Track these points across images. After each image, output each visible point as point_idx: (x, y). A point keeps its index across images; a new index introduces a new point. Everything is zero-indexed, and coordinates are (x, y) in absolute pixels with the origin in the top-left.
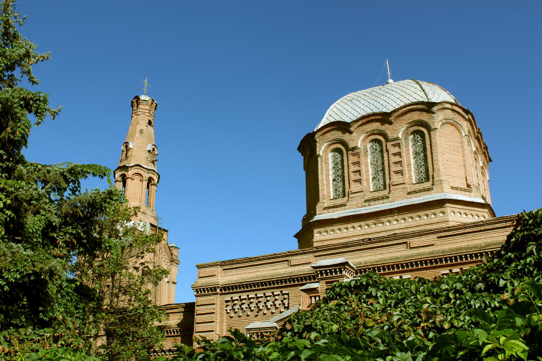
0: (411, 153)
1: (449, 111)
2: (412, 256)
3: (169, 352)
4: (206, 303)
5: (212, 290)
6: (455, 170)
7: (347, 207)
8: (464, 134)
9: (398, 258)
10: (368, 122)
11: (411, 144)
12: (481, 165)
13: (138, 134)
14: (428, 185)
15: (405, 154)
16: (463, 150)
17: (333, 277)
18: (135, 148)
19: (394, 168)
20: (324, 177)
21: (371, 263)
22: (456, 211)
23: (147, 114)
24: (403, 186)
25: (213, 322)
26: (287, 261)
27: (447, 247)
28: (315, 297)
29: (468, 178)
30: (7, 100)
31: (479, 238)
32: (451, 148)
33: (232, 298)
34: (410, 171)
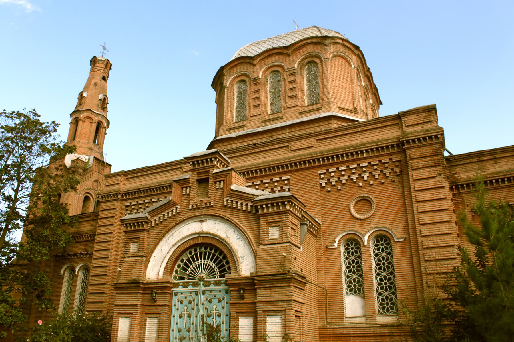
0: (305, 80)
1: (340, 46)
2: (292, 158)
3: (80, 255)
4: (108, 208)
6: (344, 96)
7: (245, 128)
8: (353, 66)
9: (278, 160)
11: (305, 73)
12: (371, 102)
15: (299, 81)
16: (352, 80)
20: (229, 104)
21: (254, 165)
23: (102, 71)
25: (112, 225)
26: (181, 168)
27: (325, 148)
28: (186, 188)
29: (355, 103)
31: (355, 138)
32: (341, 76)
33: (131, 203)
34: (303, 95)
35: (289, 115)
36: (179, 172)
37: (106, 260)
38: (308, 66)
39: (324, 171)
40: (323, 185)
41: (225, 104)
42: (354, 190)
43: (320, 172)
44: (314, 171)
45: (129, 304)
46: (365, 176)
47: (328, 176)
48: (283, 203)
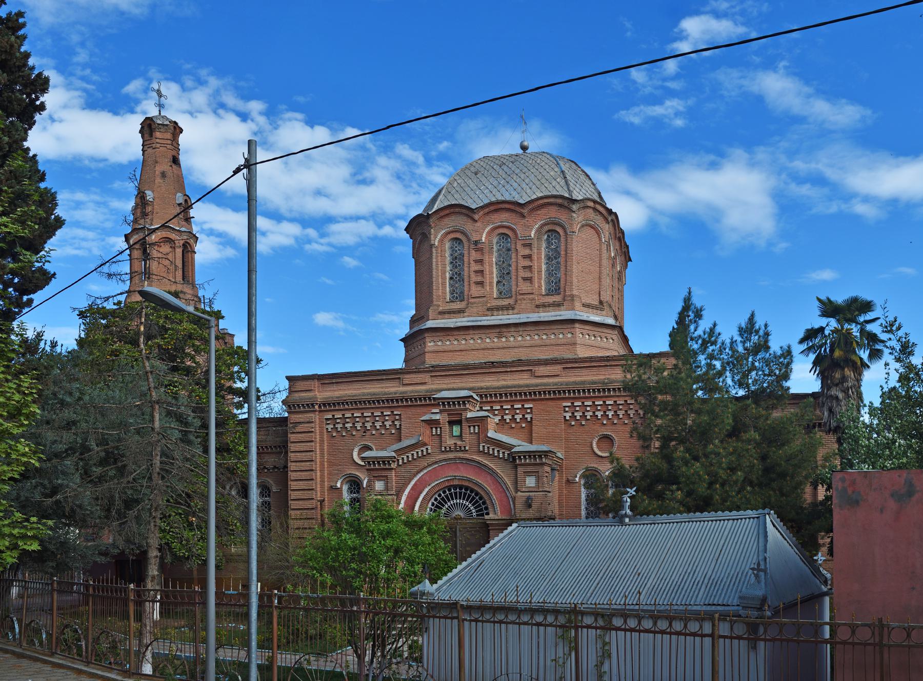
1: (591, 211)
5: (310, 406)
10: (496, 211)
11: (544, 245)
13: (158, 180)
14: (557, 298)
17: (457, 410)
18: (157, 200)
19: (523, 274)
22: (609, 336)
24: (531, 296)
30: (882, 626)
34: (540, 279)
35: (523, 306)
36: (396, 383)
37: (310, 482)
38: (548, 236)
39: (569, 404)
40: (568, 418)
41: (434, 273)
42: (597, 427)
43: (565, 404)
44: (559, 402)
45: (508, 357)
46: (610, 414)
47: (513, 412)
48: (540, 456)
